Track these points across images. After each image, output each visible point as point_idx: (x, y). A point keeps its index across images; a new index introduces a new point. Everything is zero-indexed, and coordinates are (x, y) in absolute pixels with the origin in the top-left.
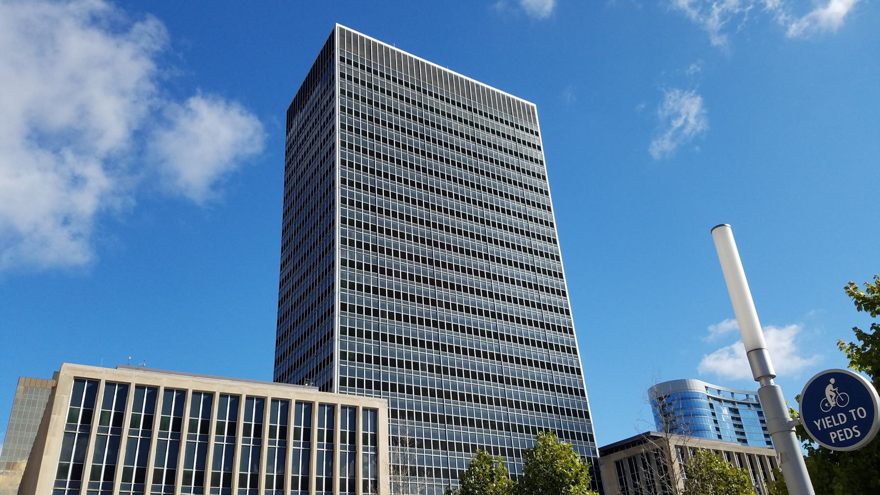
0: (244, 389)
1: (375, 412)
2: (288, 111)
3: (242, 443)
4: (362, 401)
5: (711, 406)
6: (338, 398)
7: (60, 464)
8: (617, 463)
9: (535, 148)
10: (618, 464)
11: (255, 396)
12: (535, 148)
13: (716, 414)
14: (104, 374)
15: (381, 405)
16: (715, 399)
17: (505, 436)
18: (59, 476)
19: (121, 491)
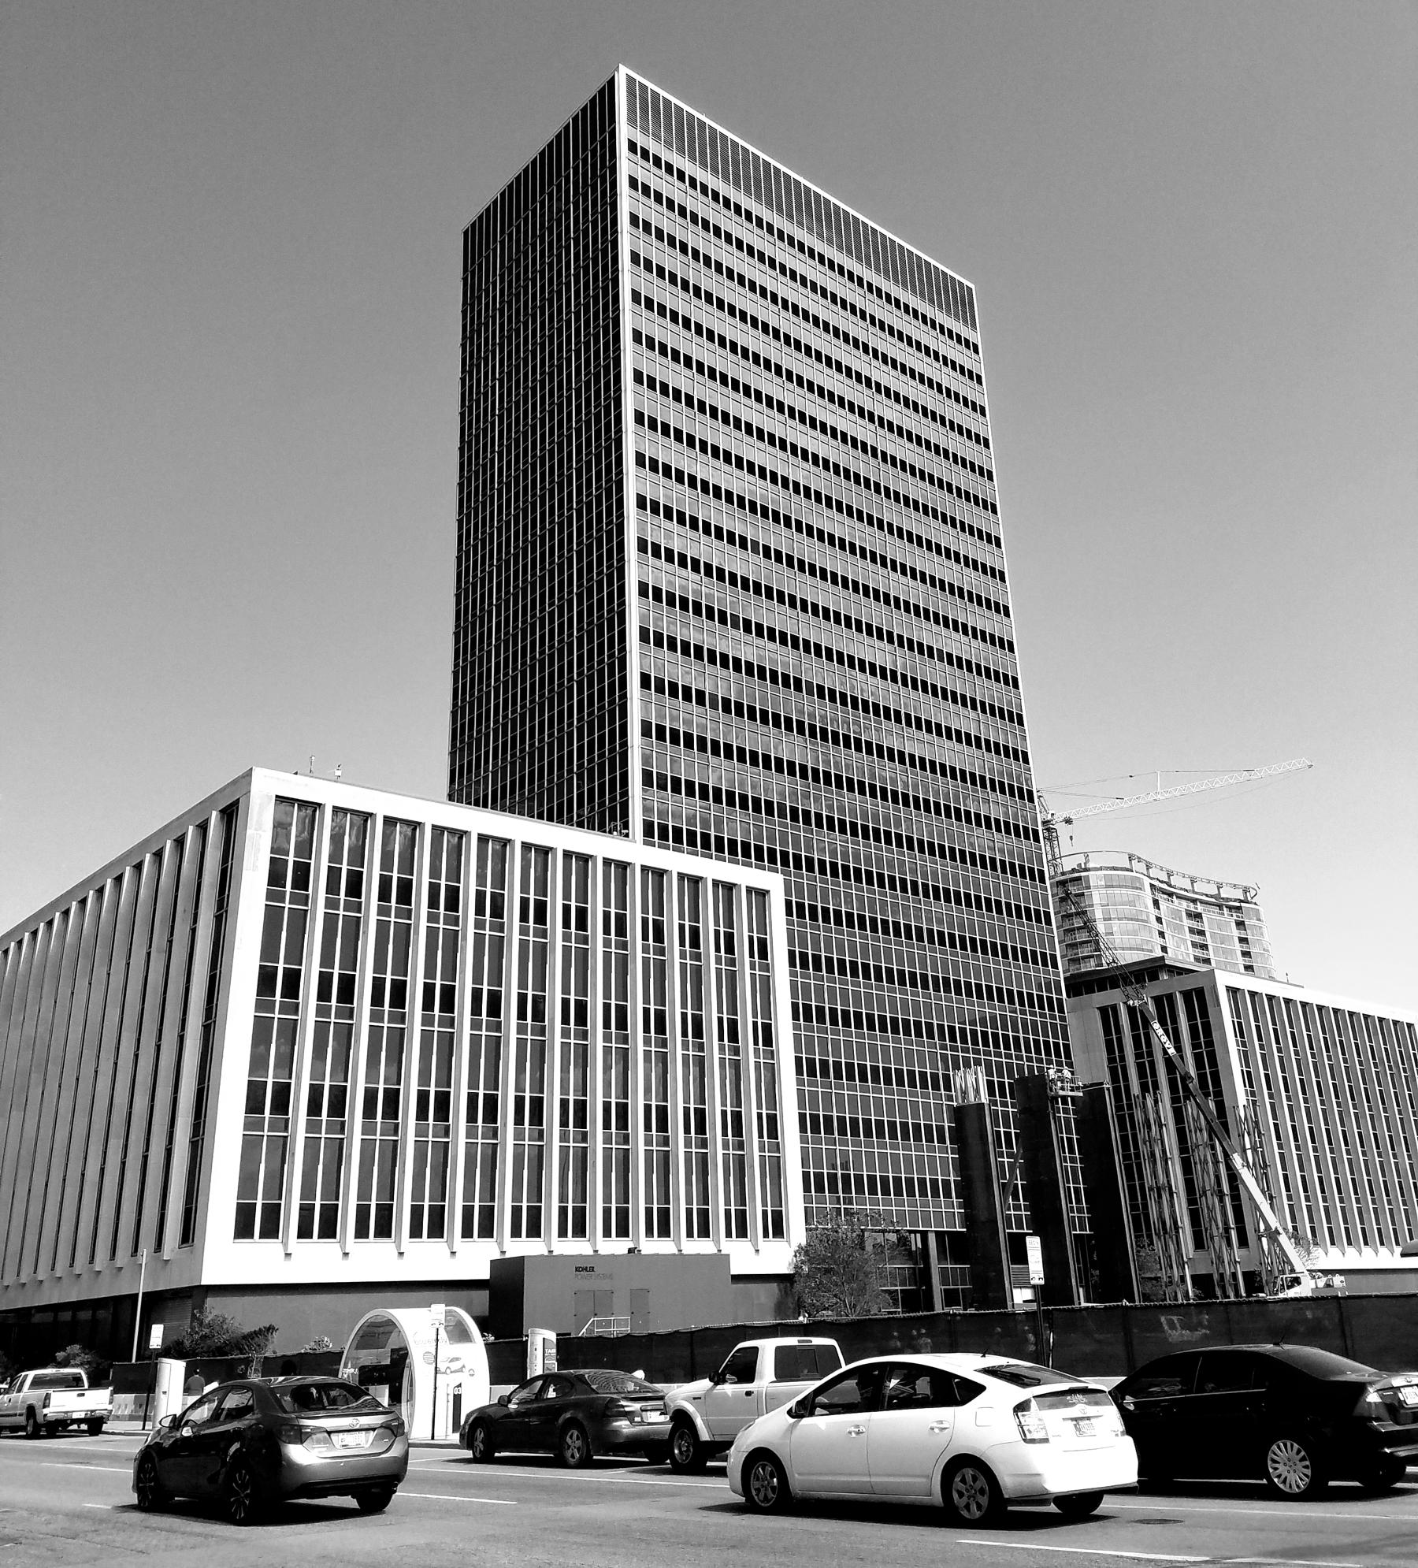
0: (381, 804)
1: (763, 894)
2: (466, 233)
3: (326, 908)
4: (745, 875)
5: (1156, 903)
6: (635, 851)
7: (261, 967)
8: (1103, 1011)
9: (779, 339)
10: (1108, 1014)
11: (574, 853)
12: (779, 339)
13: (1163, 920)
14: (329, 794)
15: (772, 881)
16: (1164, 892)
17: (809, 930)
18: (261, 991)
19: (257, 1014)
